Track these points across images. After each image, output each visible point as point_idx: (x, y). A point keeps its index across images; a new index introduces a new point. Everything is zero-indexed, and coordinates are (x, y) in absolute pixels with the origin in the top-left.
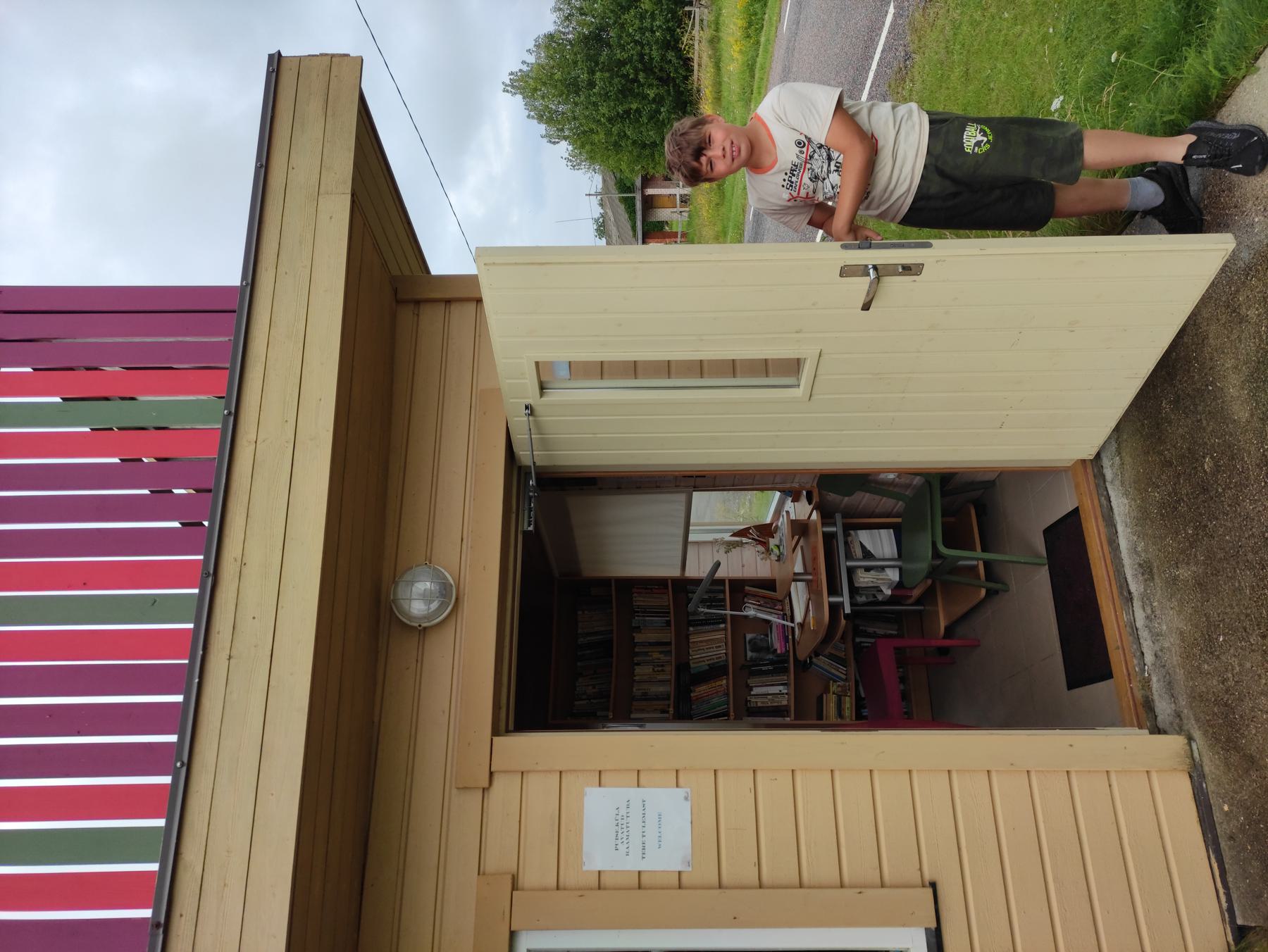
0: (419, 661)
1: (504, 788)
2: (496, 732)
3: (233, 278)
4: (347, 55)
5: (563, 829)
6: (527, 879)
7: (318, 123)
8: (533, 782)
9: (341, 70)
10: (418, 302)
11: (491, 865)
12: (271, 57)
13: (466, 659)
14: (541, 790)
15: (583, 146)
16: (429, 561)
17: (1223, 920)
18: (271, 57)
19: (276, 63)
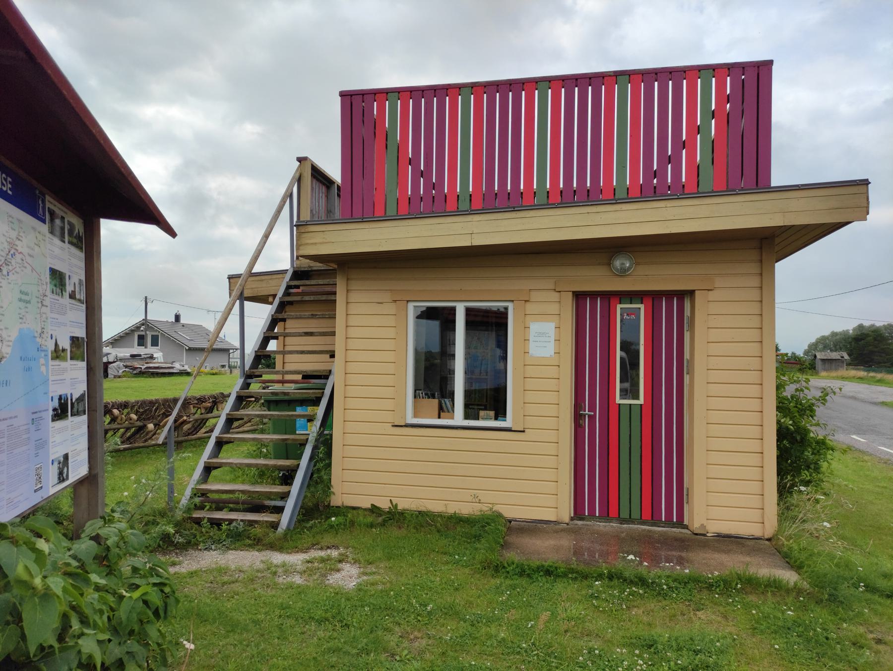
0: (599, 264)
1: (555, 296)
2: (573, 292)
3: (774, 183)
4: (868, 213)
5: (543, 316)
6: (528, 305)
7: (848, 198)
8: (556, 306)
9: (863, 212)
10: (761, 248)
11: (532, 293)
12: (867, 180)
13: (596, 279)
14: (554, 308)
15: (775, 580)
16: (637, 264)
17: (880, 381)
18: (867, 180)
19: (865, 183)
